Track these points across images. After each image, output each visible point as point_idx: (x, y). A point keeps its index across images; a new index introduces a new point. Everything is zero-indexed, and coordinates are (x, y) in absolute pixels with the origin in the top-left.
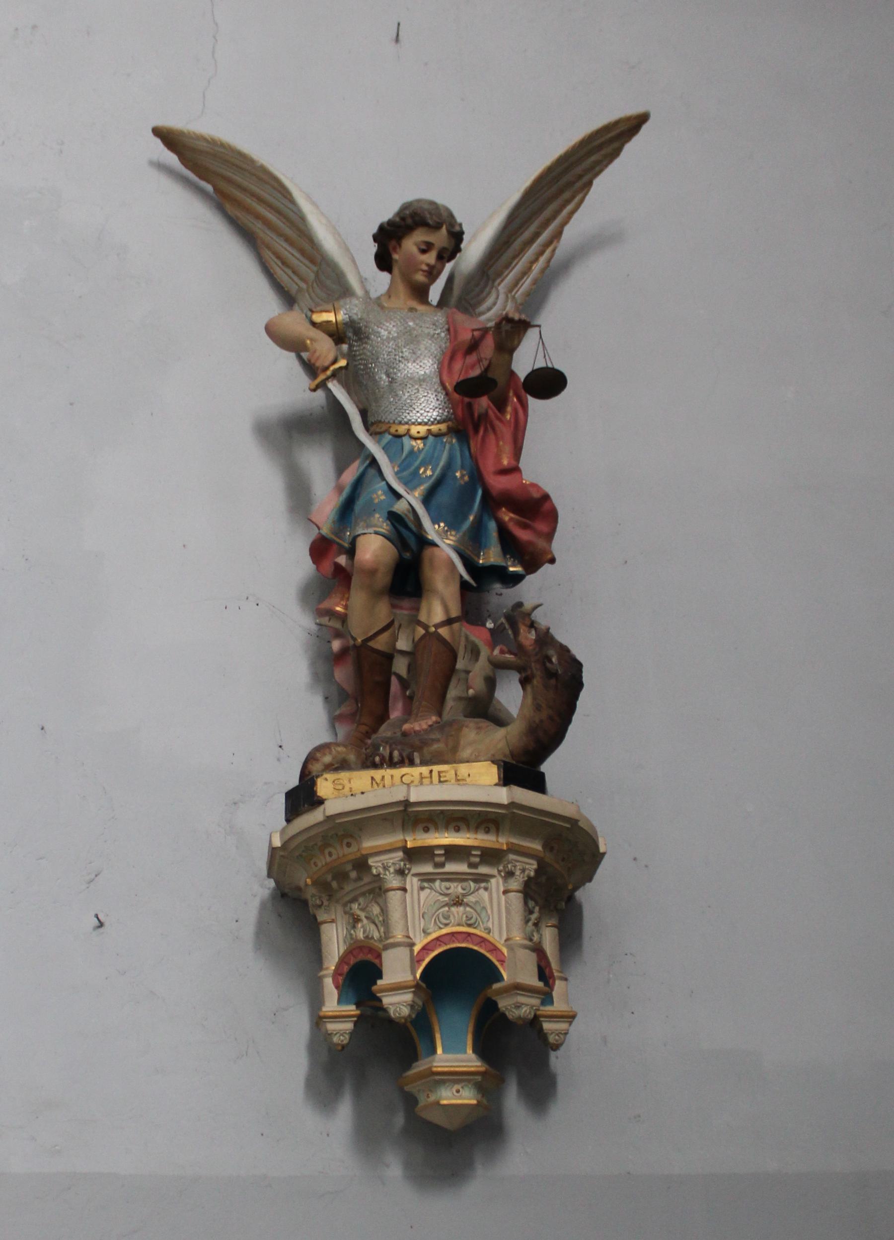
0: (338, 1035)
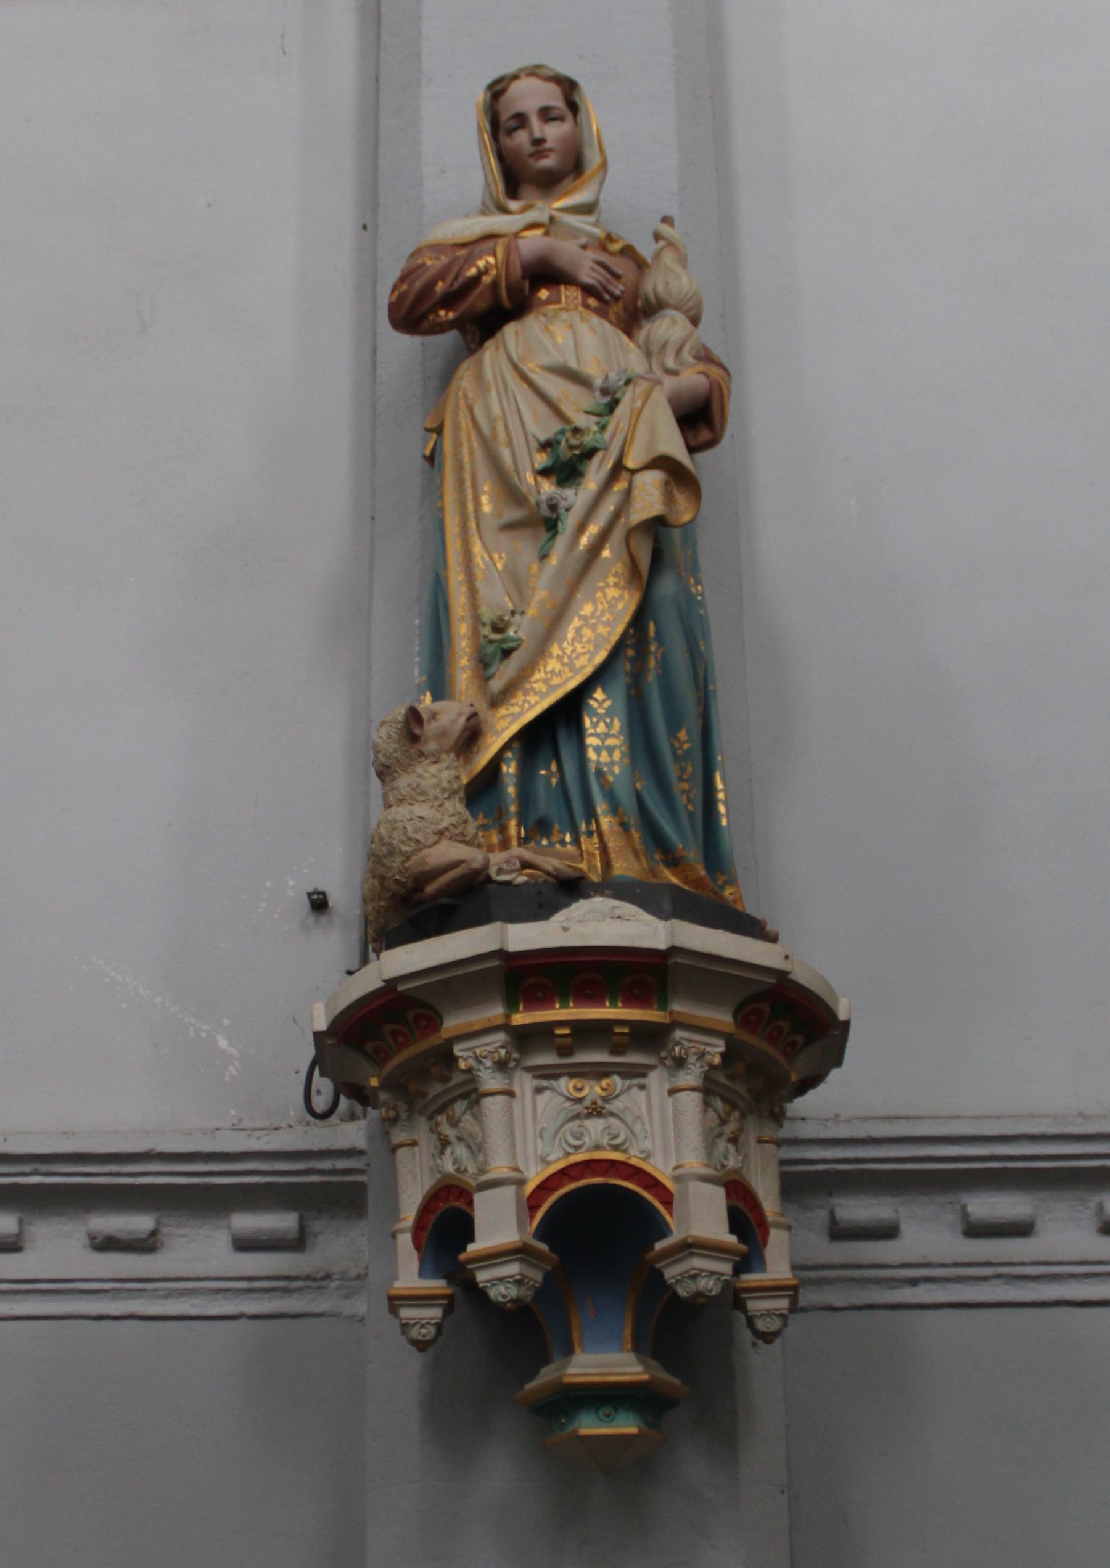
0: (418, 1326)
